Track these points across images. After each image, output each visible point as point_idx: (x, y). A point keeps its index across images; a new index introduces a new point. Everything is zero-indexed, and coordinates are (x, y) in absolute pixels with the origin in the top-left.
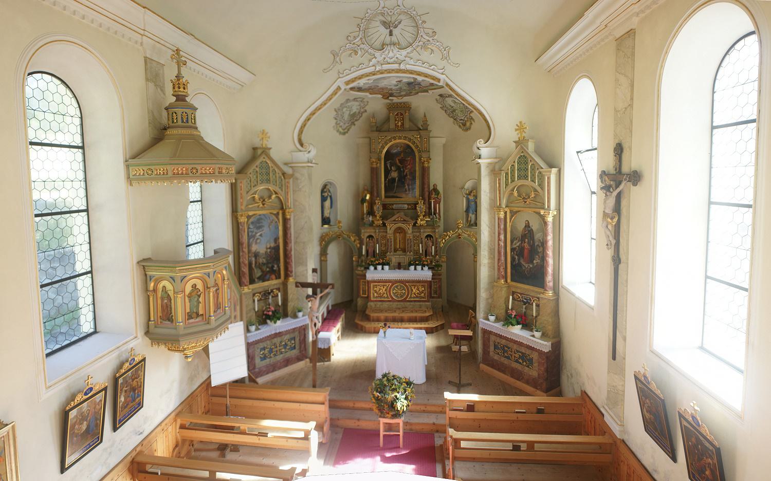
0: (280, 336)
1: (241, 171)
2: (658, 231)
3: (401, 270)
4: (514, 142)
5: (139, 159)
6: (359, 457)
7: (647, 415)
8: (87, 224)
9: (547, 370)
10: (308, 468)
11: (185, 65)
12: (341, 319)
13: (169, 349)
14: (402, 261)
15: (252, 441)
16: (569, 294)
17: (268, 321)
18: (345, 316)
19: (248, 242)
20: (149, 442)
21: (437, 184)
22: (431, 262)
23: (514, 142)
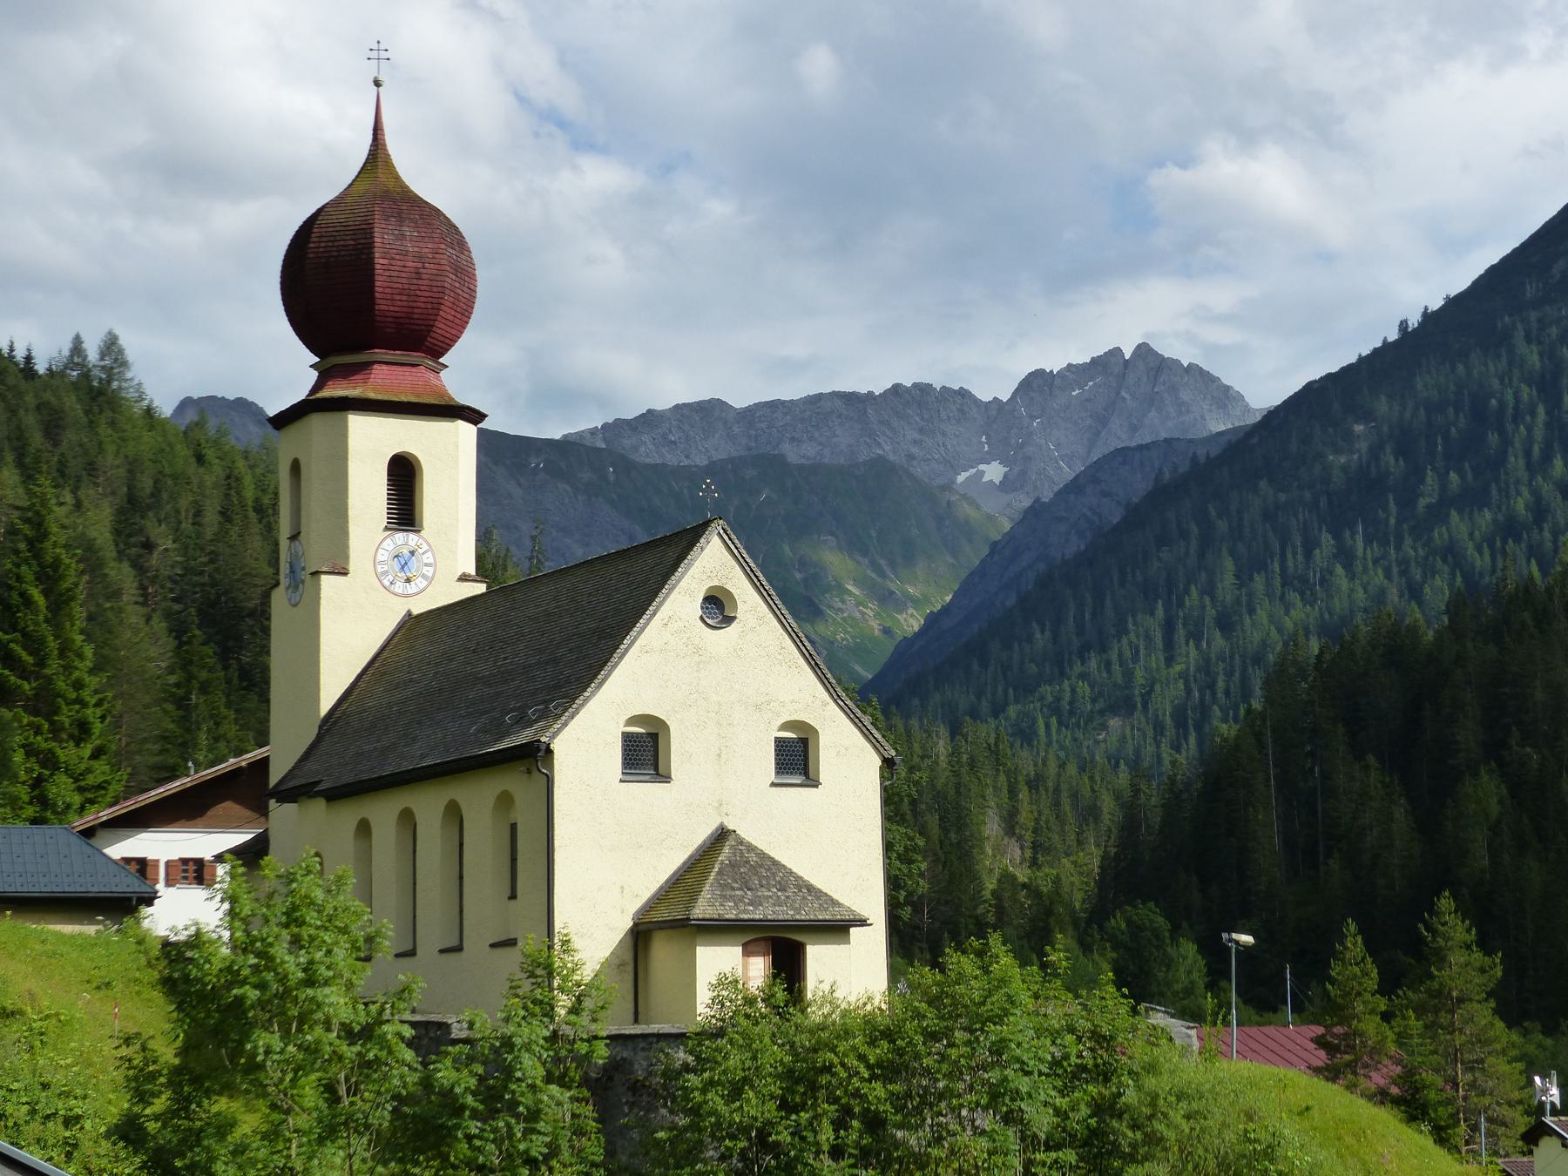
0: (1111, 664)
1: (100, 443)
2: (616, 672)
3: (1335, 1087)
4: (311, 366)
5: (59, 604)
7: (906, 913)
10: (871, 925)
11: (368, 959)
12: (333, 684)
15: (288, 518)
18: (319, 712)
19: (1158, 747)
22: (97, 1091)
23: (311, 366)
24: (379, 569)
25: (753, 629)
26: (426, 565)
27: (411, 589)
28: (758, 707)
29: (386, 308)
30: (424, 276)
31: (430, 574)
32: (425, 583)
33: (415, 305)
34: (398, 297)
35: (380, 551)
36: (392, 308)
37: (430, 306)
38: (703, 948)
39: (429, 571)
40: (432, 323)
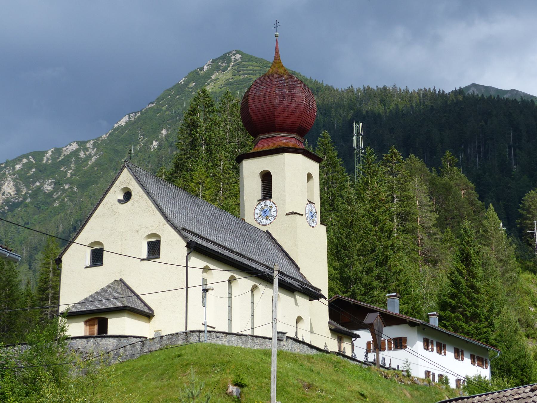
4: (298, 306)
6: (126, 314)
8: (141, 297)
9: (476, 287)
13: (146, 338)
14: (524, 334)
16: (301, 146)
17: (336, 89)
20: (89, 245)
21: (369, 85)
24: (256, 217)
25: (137, 201)
26: (274, 212)
27: (268, 222)
28: (137, 231)
29: (255, 118)
30: (266, 102)
31: (275, 215)
32: (273, 219)
33: (265, 114)
34: (258, 113)
35: (256, 210)
36: (257, 118)
37: (271, 113)
38: (419, 342)
39: (274, 214)
40: (274, 119)
